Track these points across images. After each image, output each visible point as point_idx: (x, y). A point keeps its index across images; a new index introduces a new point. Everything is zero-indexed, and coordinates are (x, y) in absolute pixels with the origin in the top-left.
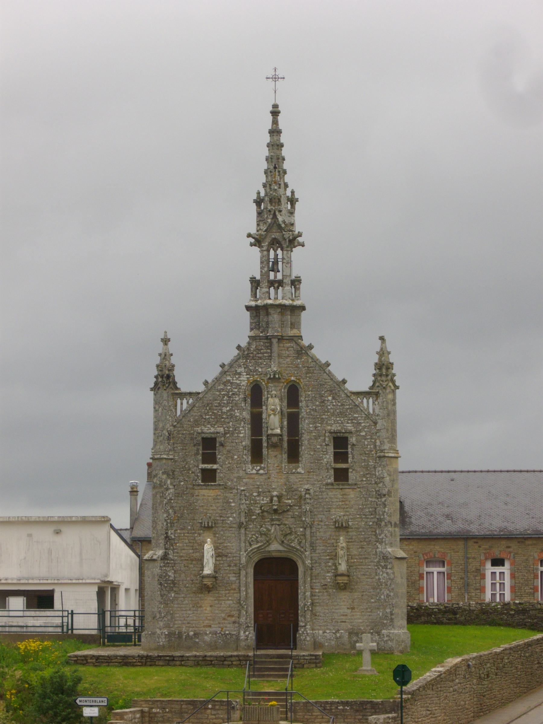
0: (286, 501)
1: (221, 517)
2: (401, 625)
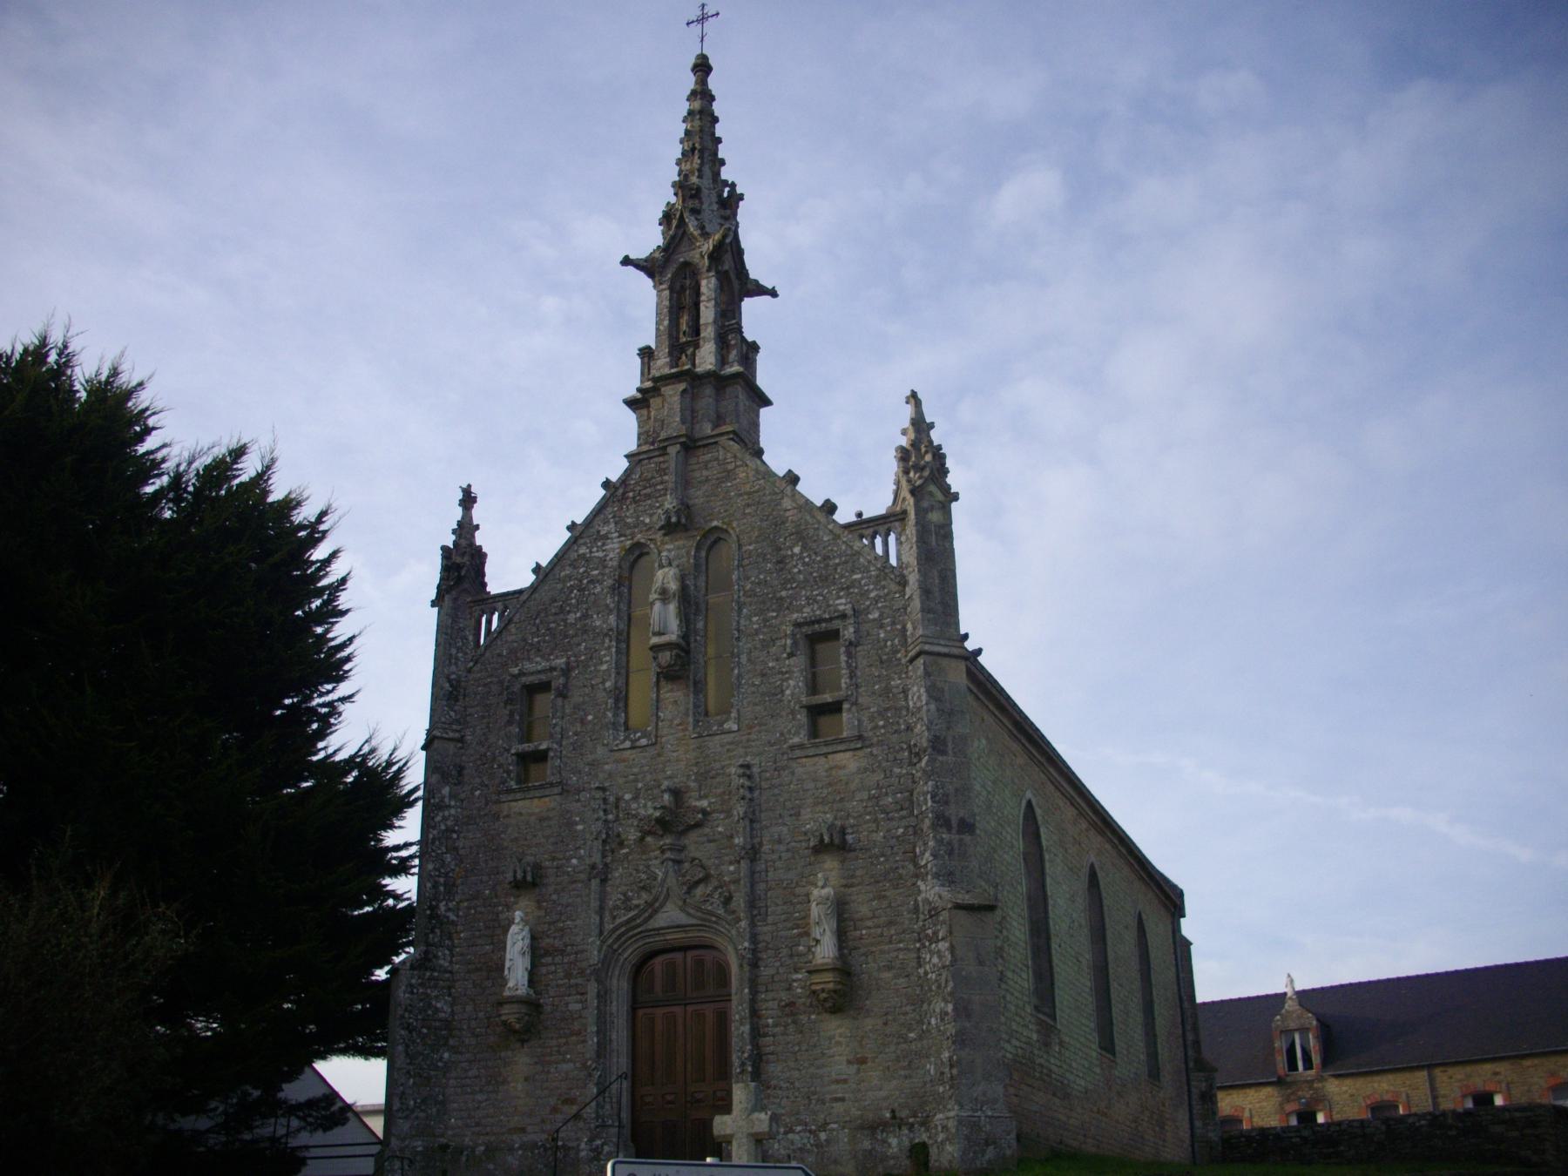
0: (698, 804)
1: (554, 859)
2: (984, 1094)
